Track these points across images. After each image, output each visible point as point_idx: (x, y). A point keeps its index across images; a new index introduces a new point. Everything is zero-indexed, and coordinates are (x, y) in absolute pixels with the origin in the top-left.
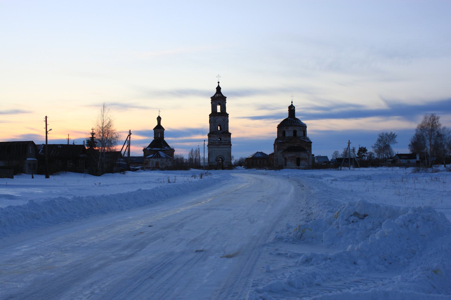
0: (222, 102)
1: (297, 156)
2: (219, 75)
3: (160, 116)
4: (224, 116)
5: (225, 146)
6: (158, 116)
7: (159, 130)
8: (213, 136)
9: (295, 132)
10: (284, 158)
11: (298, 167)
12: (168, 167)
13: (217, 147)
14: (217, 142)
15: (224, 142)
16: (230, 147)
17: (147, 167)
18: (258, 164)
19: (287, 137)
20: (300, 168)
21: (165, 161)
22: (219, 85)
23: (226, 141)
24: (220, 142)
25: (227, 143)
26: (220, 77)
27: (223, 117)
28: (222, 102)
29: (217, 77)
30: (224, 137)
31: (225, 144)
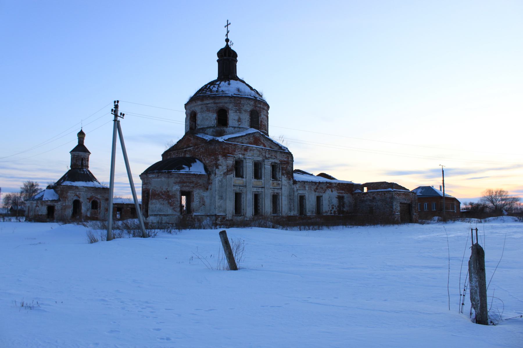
3: (83, 131)
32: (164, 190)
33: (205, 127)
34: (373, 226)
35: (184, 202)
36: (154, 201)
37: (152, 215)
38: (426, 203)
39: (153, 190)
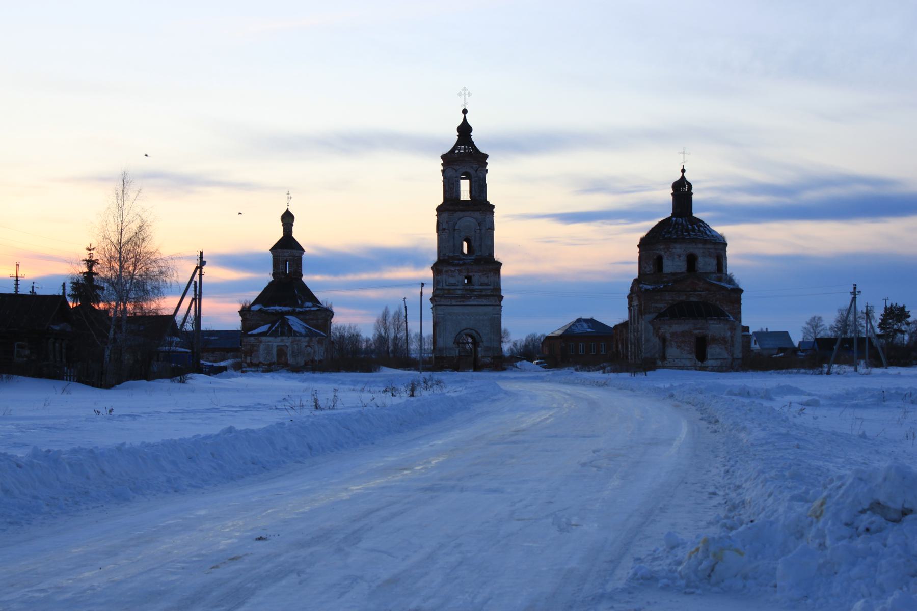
0: (476, 171)
1: (696, 332)
2: (465, 89)
7: (287, 253)
8: (447, 271)
9: (691, 260)
11: (700, 364)
12: (313, 361)
13: (458, 303)
14: (458, 287)
15: (481, 287)
16: (497, 303)
17: (251, 362)
22: (465, 118)
23: (486, 284)
25: (489, 293)
26: (469, 94)
27: (477, 215)
28: (476, 171)
29: (460, 94)
30: (480, 274)
31: (484, 293)
32: (723, 335)
33: (708, 271)
34: (762, 372)
35: (431, 340)
36: (713, 346)
38: (582, 344)
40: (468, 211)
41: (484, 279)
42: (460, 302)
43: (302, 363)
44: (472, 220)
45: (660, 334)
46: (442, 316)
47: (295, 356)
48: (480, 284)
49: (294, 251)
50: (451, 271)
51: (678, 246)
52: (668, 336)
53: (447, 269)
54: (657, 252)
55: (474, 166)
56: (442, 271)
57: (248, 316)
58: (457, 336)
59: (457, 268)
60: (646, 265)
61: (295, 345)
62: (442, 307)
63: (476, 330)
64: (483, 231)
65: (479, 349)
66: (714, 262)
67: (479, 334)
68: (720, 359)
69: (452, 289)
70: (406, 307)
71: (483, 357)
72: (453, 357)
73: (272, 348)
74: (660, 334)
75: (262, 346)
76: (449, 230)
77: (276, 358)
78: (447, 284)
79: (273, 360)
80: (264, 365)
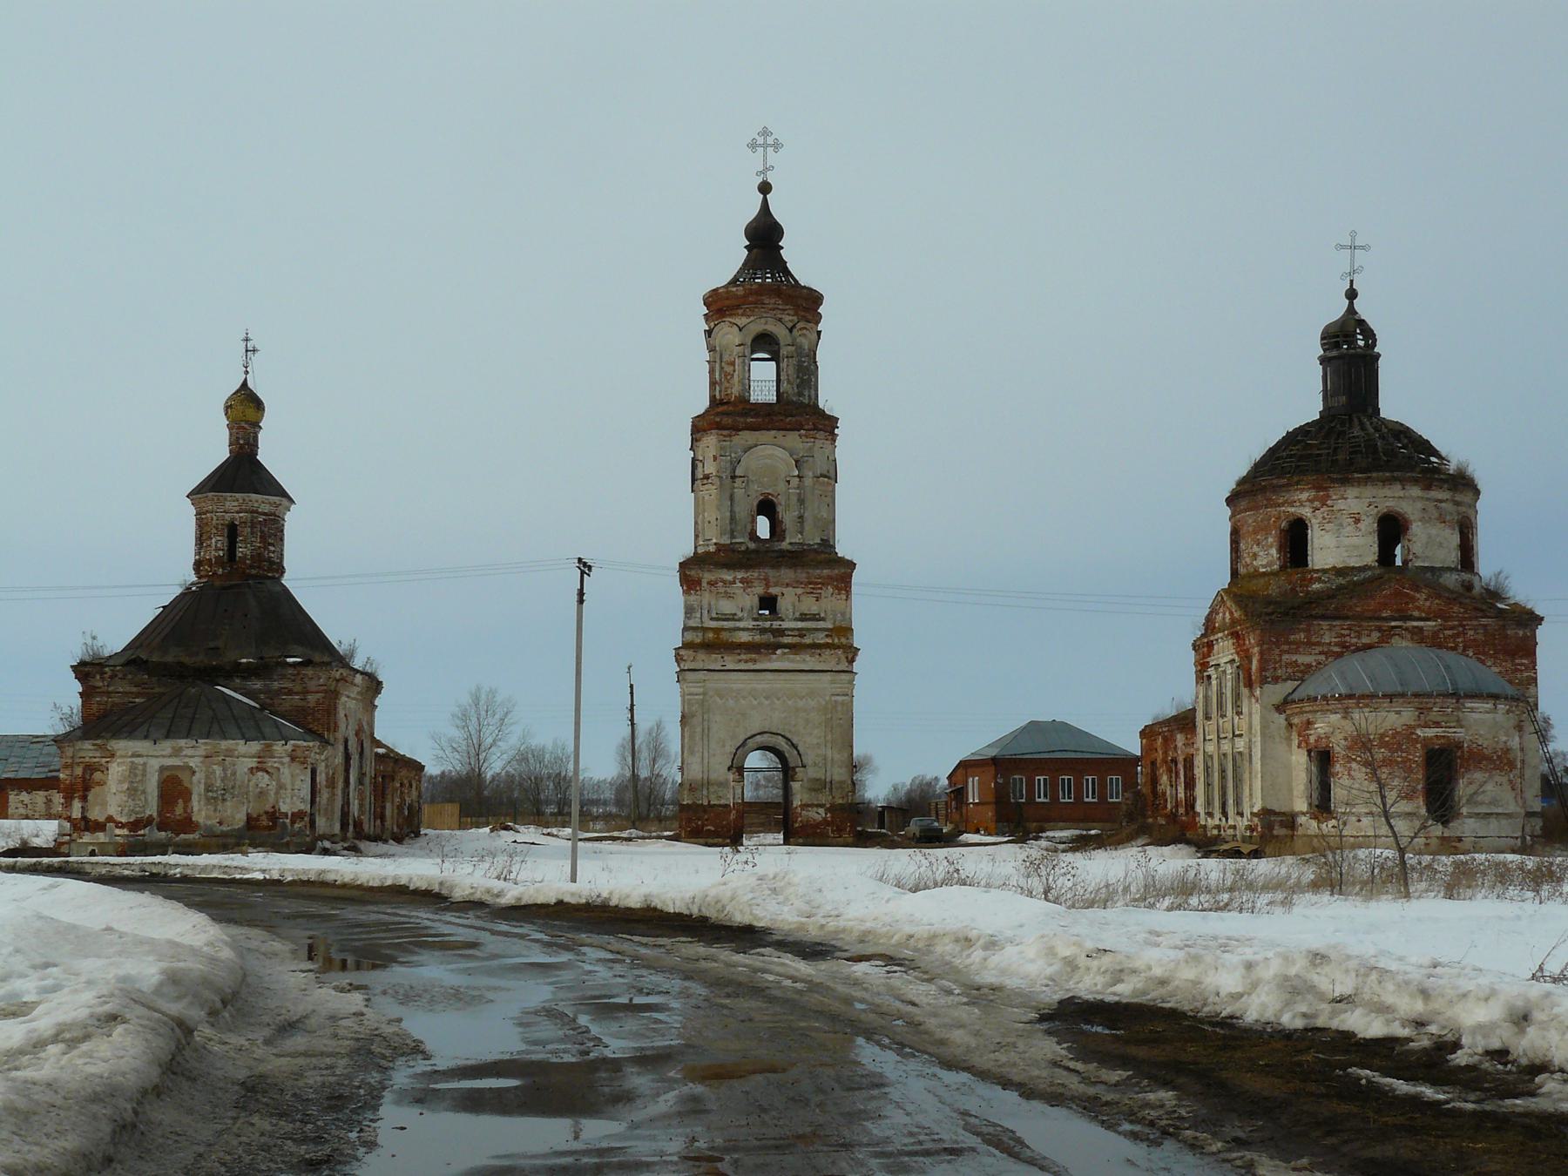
0: (791, 330)
1: (1430, 732)
2: (765, 133)
3: (250, 385)
4: (797, 428)
5: (808, 661)
6: (237, 386)
7: (232, 504)
8: (711, 584)
9: (1391, 529)
10: (1309, 752)
11: (1437, 830)
12: (274, 815)
13: (742, 666)
14: (741, 625)
15: (800, 625)
16: (844, 666)
17: (84, 818)
18: (1042, 800)
19: (1325, 571)
20: (1460, 839)
21: (253, 763)
22: (765, 204)
23: (815, 617)
24: (767, 624)
25: (821, 638)
26: (777, 146)
27: (793, 439)
28: (791, 330)
29: (753, 146)
30: (799, 591)
31: (807, 640)
33: (1438, 565)
37: (1470, 816)
39: (1475, 745)
40: (768, 430)
41: (810, 605)
42: (746, 662)
43: (239, 819)
44: (779, 452)
45: (1312, 740)
46: (701, 697)
47: (214, 798)
48: (797, 615)
49: (254, 496)
50: (724, 582)
51: (1351, 492)
52: (1338, 746)
53: (713, 578)
54: (1292, 510)
55: (786, 318)
56: (699, 582)
57: (97, 682)
58: (737, 750)
59: (740, 575)
60: (1256, 549)
61: (215, 767)
62: (700, 675)
63: (788, 735)
64: (808, 482)
65: (795, 786)
66: (1455, 539)
67: (795, 747)
68: (1497, 814)
69: (725, 630)
70: (631, 686)
71: (805, 806)
72: (726, 806)
73: (144, 775)
74: (1312, 740)
75: (116, 770)
76: (720, 477)
77: (155, 808)
78: (714, 615)
79: (148, 813)
80: (117, 827)
